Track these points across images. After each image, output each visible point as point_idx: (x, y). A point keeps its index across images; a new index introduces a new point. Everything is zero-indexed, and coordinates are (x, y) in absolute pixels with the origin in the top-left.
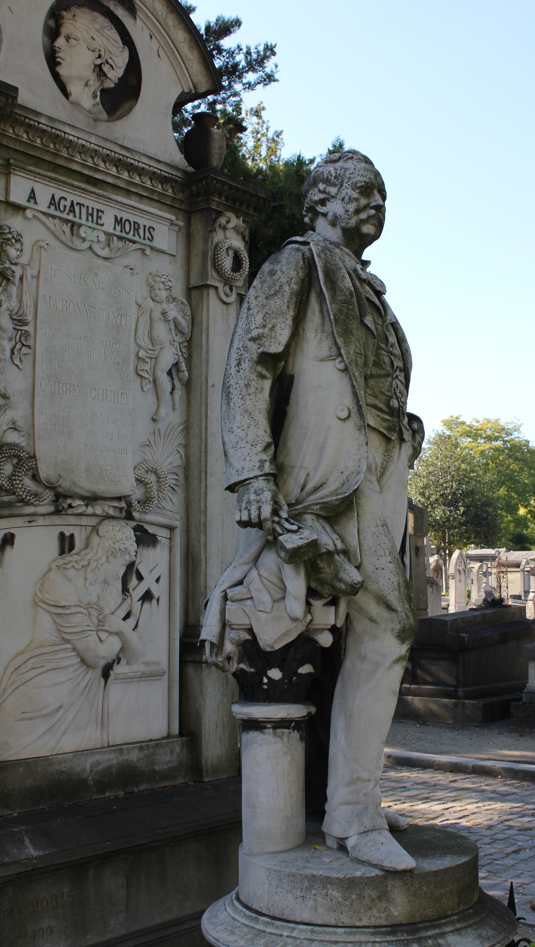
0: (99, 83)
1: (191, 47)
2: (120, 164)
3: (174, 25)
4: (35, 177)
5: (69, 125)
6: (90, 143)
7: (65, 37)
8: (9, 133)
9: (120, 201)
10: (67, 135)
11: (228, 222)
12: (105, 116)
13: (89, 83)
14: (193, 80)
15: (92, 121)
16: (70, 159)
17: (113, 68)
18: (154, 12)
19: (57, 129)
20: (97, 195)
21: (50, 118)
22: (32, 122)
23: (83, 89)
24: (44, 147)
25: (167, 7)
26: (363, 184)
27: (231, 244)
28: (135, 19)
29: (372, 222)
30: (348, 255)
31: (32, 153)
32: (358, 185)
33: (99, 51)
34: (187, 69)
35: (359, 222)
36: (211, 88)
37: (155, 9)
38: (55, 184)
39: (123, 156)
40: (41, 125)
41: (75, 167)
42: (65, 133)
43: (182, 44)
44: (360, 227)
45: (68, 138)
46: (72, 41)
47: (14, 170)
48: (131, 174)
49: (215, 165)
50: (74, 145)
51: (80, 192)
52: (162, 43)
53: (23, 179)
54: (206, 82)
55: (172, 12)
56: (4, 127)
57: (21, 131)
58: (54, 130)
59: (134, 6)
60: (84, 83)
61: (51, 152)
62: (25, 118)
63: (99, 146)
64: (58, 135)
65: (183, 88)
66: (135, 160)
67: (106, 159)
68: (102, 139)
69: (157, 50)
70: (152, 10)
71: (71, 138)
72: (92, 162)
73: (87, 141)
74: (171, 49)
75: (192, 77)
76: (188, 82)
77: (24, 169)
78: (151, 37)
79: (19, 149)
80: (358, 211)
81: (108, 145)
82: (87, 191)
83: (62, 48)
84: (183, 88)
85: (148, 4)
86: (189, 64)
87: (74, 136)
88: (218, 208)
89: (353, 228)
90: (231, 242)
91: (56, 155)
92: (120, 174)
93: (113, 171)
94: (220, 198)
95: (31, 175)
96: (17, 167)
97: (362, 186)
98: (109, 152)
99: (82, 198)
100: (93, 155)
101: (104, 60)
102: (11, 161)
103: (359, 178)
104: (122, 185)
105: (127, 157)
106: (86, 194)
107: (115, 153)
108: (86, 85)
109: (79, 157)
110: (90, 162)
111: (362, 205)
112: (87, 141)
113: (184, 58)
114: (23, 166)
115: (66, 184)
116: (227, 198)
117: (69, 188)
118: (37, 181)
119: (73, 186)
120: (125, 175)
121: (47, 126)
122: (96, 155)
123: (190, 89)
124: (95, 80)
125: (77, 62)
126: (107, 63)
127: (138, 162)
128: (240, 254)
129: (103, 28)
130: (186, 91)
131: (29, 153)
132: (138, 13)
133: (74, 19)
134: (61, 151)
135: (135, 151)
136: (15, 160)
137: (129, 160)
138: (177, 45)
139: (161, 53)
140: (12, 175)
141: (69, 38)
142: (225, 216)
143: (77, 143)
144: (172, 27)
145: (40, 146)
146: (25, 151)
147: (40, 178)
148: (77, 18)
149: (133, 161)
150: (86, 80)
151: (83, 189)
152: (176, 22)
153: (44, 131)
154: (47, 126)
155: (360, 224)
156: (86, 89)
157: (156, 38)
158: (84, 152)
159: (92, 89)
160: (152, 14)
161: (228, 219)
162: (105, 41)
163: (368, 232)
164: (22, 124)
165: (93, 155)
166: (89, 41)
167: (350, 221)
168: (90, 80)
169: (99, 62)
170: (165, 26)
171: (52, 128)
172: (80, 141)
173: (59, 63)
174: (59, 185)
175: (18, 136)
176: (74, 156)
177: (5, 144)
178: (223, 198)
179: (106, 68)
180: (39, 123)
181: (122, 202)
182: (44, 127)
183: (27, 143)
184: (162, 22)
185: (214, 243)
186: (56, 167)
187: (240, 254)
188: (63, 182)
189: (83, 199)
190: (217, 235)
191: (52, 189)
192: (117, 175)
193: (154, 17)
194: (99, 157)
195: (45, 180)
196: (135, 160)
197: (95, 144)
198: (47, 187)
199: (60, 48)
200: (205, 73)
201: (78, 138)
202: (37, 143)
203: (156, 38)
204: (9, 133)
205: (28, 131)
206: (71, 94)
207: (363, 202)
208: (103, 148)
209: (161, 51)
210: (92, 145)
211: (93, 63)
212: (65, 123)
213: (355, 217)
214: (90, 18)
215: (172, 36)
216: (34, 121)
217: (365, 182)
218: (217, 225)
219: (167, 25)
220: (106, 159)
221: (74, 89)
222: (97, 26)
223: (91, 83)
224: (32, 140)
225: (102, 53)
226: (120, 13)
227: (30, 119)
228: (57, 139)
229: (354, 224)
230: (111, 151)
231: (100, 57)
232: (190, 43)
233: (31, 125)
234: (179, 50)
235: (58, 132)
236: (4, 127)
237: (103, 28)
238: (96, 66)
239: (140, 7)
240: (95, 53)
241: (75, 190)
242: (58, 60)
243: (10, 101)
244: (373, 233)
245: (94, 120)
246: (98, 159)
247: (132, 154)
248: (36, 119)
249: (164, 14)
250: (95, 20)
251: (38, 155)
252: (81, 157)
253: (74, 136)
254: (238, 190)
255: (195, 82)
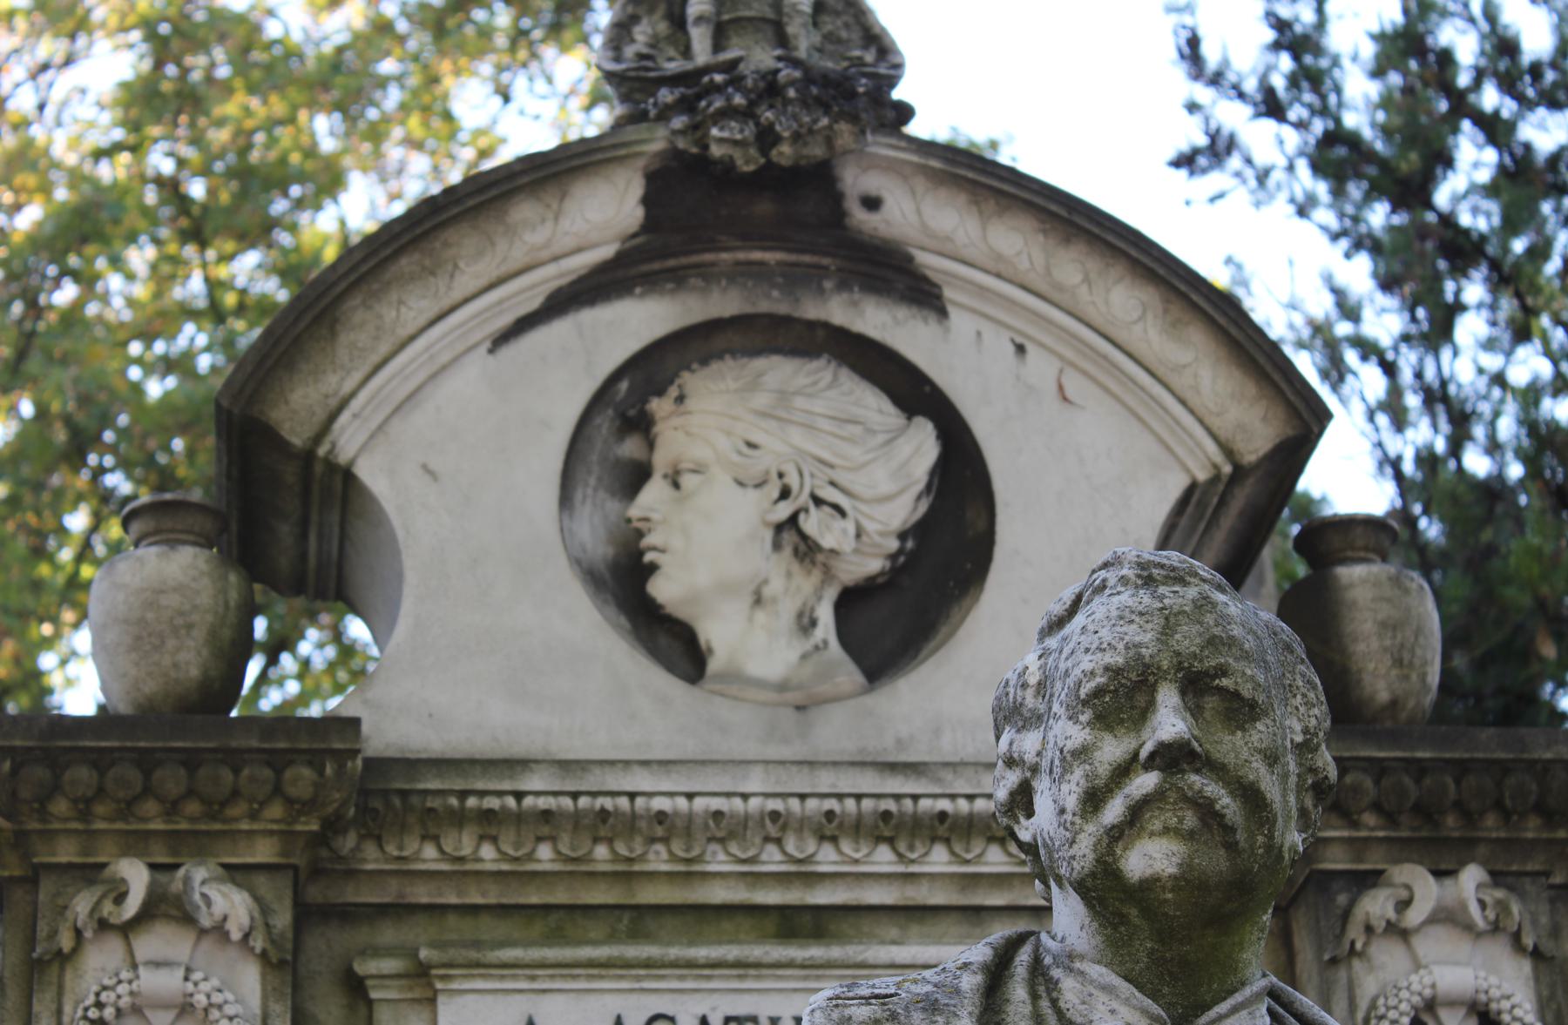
0: (817, 575)
1: (1174, 324)
2: (889, 828)
3: (1086, 279)
4: (533, 978)
5: (645, 763)
6: (745, 797)
7: (665, 476)
8: (424, 861)
9: (908, 961)
10: (640, 801)
11: (1404, 905)
12: (850, 675)
13: (767, 591)
14: (1215, 429)
15: (790, 713)
16: (689, 874)
17: (842, 512)
18: (1002, 268)
19: (594, 794)
20: (803, 966)
21: (566, 766)
22: (493, 803)
23: (750, 619)
24: (570, 868)
25: (1045, 232)
26: (1100, 680)
27: (1433, 986)
28: (942, 313)
29: (1157, 825)
30: (1107, 989)
31: (534, 899)
32: (1083, 693)
33: (781, 475)
34: (1183, 402)
35: (1106, 840)
36: (1290, 432)
37: (999, 257)
38: (621, 977)
39: (897, 797)
40: (528, 801)
41: (719, 894)
42: (632, 796)
43: (1138, 328)
44: (1116, 861)
45: (648, 810)
46: (688, 481)
47: (444, 978)
48: (958, 848)
49: (1383, 696)
50: (679, 823)
51: (728, 977)
52: (1069, 354)
53: (489, 998)
54: (1264, 419)
55: (1067, 240)
56: (401, 848)
57: (412, 846)
58: (583, 802)
59: (925, 279)
60: (749, 600)
61: (604, 874)
62: (463, 794)
63: (784, 796)
64: (603, 811)
65: (1188, 470)
66: (953, 797)
67: (829, 829)
68: (794, 769)
69: (1053, 388)
70: (991, 265)
71: (660, 804)
72: (778, 856)
73: (728, 795)
74: (1105, 357)
75: (1209, 420)
76: (1199, 445)
77: (478, 965)
78: (1021, 349)
79: (479, 900)
80: (1093, 800)
81: (826, 781)
82: (758, 965)
83: (655, 516)
84: (1188, 470)
85: (970, 253)
86: (1180, 382)
87: (671, 794)
88: (1361, 861)
89: (1093, 875)
90: (1427, 980)
91: (627, 877)
92: (913, 861)
93: (883, 859)
94: (1355, 825)
95: (514, 977)
96: (450, 965)
97: (1098, 692)
98: (831, 804)
99: (747, 997)
100: (773, 830)
101: (804, 498)
102: (424, 954)
103: (1086, 663)
104: (939, 897)
105: (915, 798)
106: (758, 977)
107: (858, 797)
108: (758, 601)
109: (722, 856)
110: (772, 859)
111: (1104, 770)
112: (728, 795)
113: (1160, 372)
114: (473, 955)
115: (664, 966)
116: (1390, 819)
117: (681, 978)
118: (544, 991)
119: (691, 964)
120: (939, 860)
121: (556, 794)
122: (784, 828)
123: (1215, 466)
124: (789, 575)
125: (707, 544)
126: (818, 501)
127: (971, 797)
128: (1499, 1013)
129: (783, 396)
130: (1202, 476)
131: (522, 900)
132: (948, 293)
133: (682, 408)
134: (642, 858)
135: (946, 765)
136: (433, 945)
137: (925, 804)
138: (1121, 336)
139: (1073, 384)
140: (441, 999)
141: (677, 472)
142: (1391, 885)
143: (690, 817)
144: (1084, 289)
145: (557, 867)
146: (504, 901)
147: (552, 977)
148: (690, 403)
149: (944, 805)
150: (752, 587)
151: (738, 964)
152: (1094, 264)
153: (546, 815)
154: (556, 794)
155: (1110, 850)
156: (761, 616)
157: (1042, 345)
158: (731, 835)
159: (788, 610)
160: (998, 276)
161: (1404, 894)
162: (797, 437)
163: (1149, 872)
164: (459, 819)
165: (773, 830)
166: (735, 458)
167: (1075, 850)
168: (766, 582)
169: (784, 511)
170: (1056, 296)
171: (575, 795)
172: (700, 804)
173: (653, 568)
174: (638, 978)
175: (461, 859)
176: (698, 859)
177: (424, 900)
178: (1369, 819)
179: (812, 523)
180: (519, 795)
181: (920, 961)
182: (543, 803)
183: (500, 873)
184: (1043, 287)
185: (1363, 1005)
186: (640, 920)
187: (1499, 1013)
188: (648, 964)
189: (754, 998)
190: (1371, 969)
191: (608, 998)
192: (900, 869)
193: (1011, 281)
194: (800, 830)
195: (574, 977)
196: (953, 797)
197: (767, 795)
198: (592, 998)
199: (646, 520)
200: (1251, 388)
201: (690, 796)
202: (539, 861)
203: (1042, 345)
204: (424, 861)
205: (493, 832)
206: (710, 650)
207: (1112, 750)
208: (803, 797)
209: (1073, 384)
210: (754, 803)
211: (766, 524)
212: (627, 763)
213: (1091, 828)
214: (732, 385)
215: (1092, 315)
216: (500, 794)
217: (1107, 669)
218: (1355, 932)
219: (1060, 288)
220: (829, 829)
221: (721, 633)
222: (762, 400)
223: (775, 586)
224: (516, 859)
225: (793, 480)
226: (878, 320)
227: (482, 794)
228: (603, 825)
229: (1091, 856)
230: (840, 797)
231: (785, 494)
232: (1166, 311)
233: (490, 811)
234: (1131, 349)
235: (600, 802)
236: (401, 848)
237: (783, 396)
238: (779, 528)
239: (946, 273)
240: (766, 489)
241: (709, 978)
242: (649, 557)
243: (329, 770)
244: (1172, 870)
245: (800, 708)
246: (801, 838)
247: (939, 781)
248: (506, 786)
249: (1039, 258)
250: (753, 386)
251: (561, 896)
252: (729, 854)
253: (671, 794)
254: (1419, 769)
255: (1222, 434)
